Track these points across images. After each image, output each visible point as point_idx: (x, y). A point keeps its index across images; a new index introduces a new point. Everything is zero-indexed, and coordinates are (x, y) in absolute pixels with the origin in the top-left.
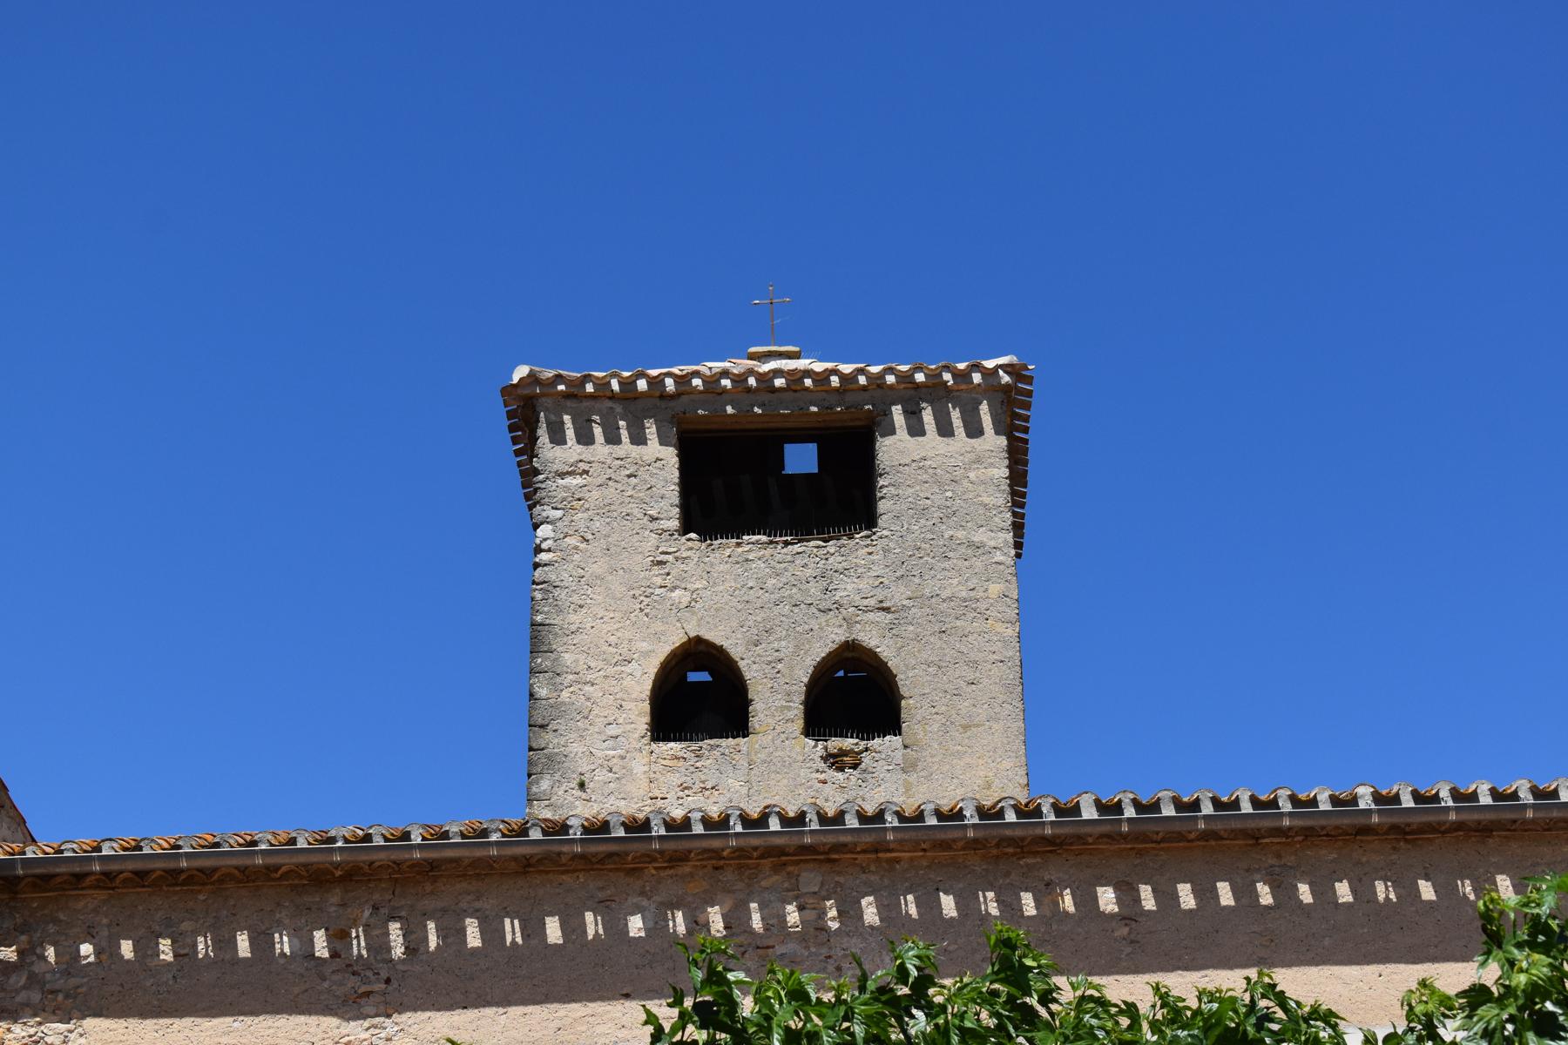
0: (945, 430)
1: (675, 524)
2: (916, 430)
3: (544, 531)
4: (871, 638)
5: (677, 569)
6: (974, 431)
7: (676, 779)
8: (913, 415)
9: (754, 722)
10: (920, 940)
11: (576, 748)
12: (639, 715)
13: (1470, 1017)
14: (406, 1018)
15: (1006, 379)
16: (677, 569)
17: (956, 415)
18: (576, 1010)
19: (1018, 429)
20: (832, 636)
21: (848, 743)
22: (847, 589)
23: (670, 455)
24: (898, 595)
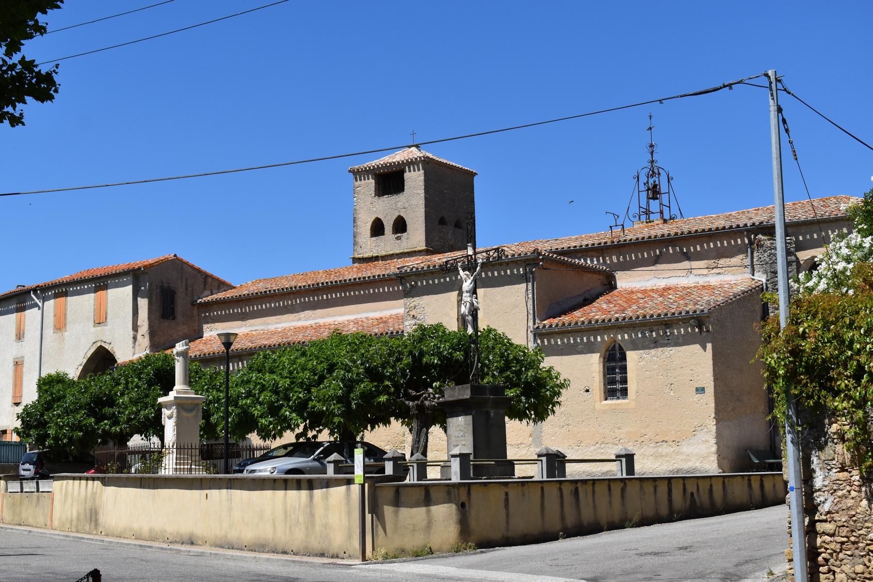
0: (414, 170)
1: (374, 195)
2: (410, 171)
3: (355, 199)
4: (402, 215)
5: (374, 204)
6: (419, 170)
7: (374, 245)
8: (409, 168)
9: (385, 233)
10: (198, 335)
11: (360, 240)
12: (368, 233)
13: (277, 386)
14: (249, 321)
15: (423, 159)
16: (374, 204)
17: (416, 167)
18: (266, 318)
19: (409, 168)
20: (397, 214)
21: (399, 235)
22: (399, 205)
23: (373, 181)
24: (406, 205)
